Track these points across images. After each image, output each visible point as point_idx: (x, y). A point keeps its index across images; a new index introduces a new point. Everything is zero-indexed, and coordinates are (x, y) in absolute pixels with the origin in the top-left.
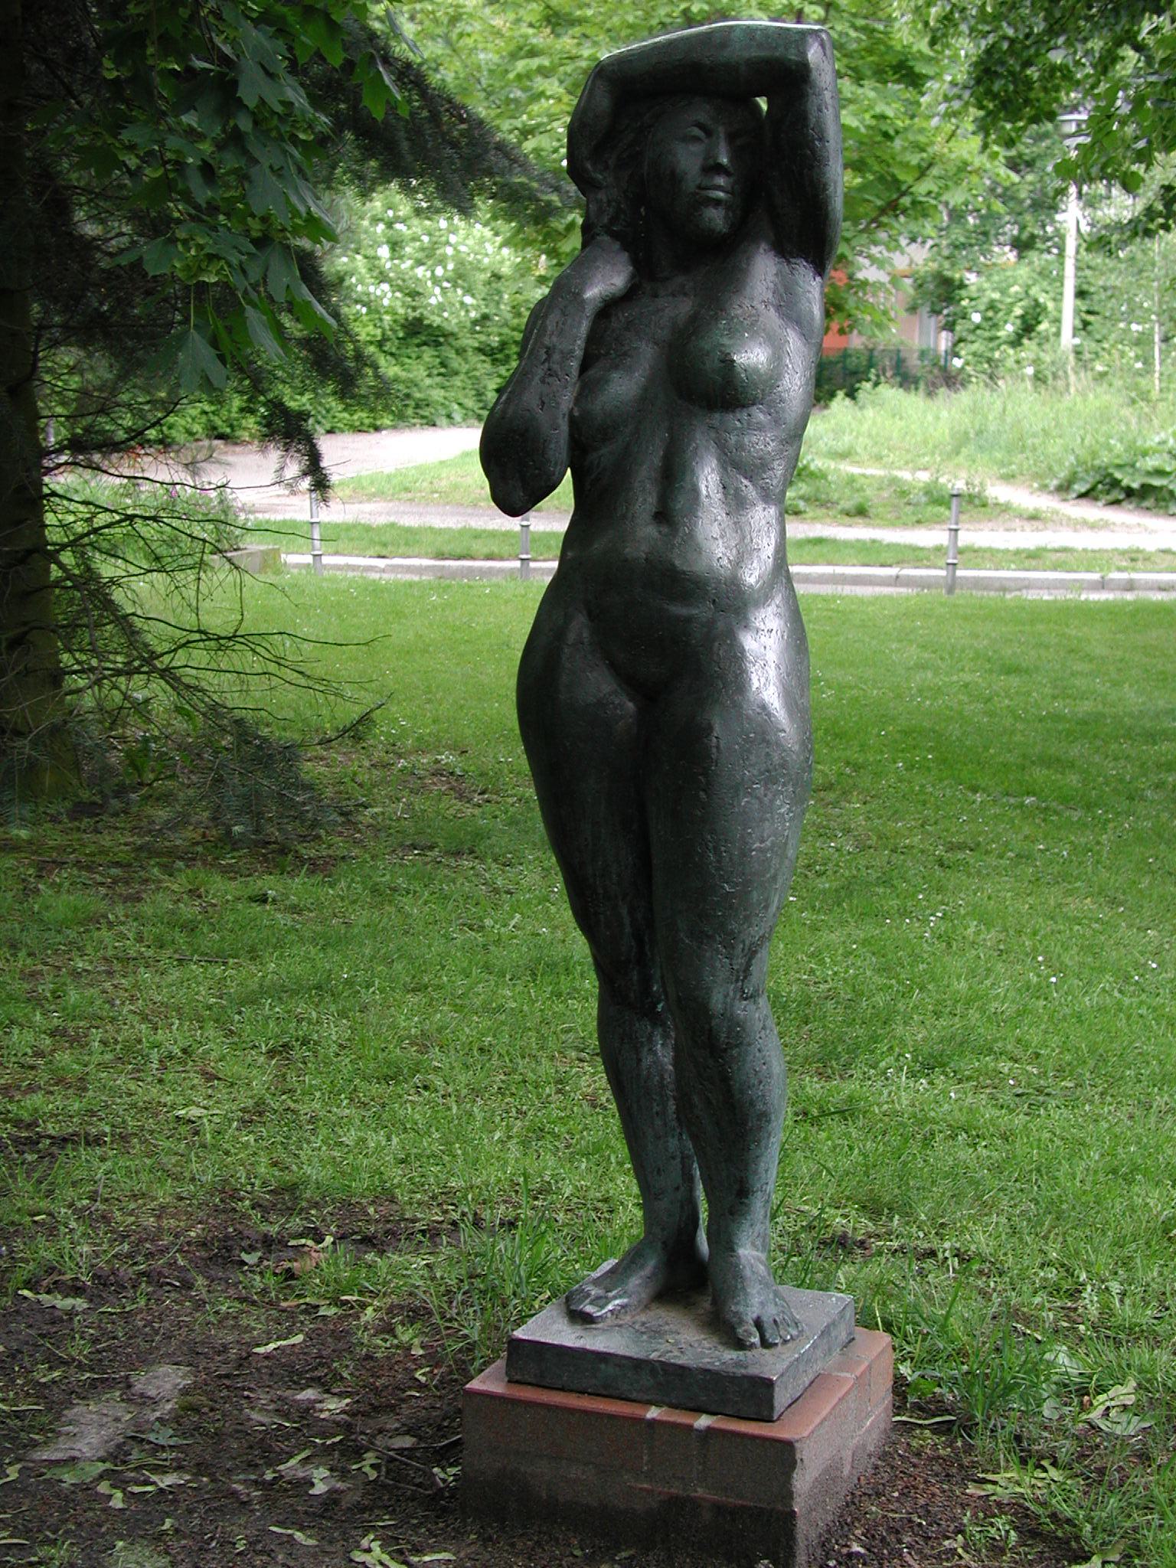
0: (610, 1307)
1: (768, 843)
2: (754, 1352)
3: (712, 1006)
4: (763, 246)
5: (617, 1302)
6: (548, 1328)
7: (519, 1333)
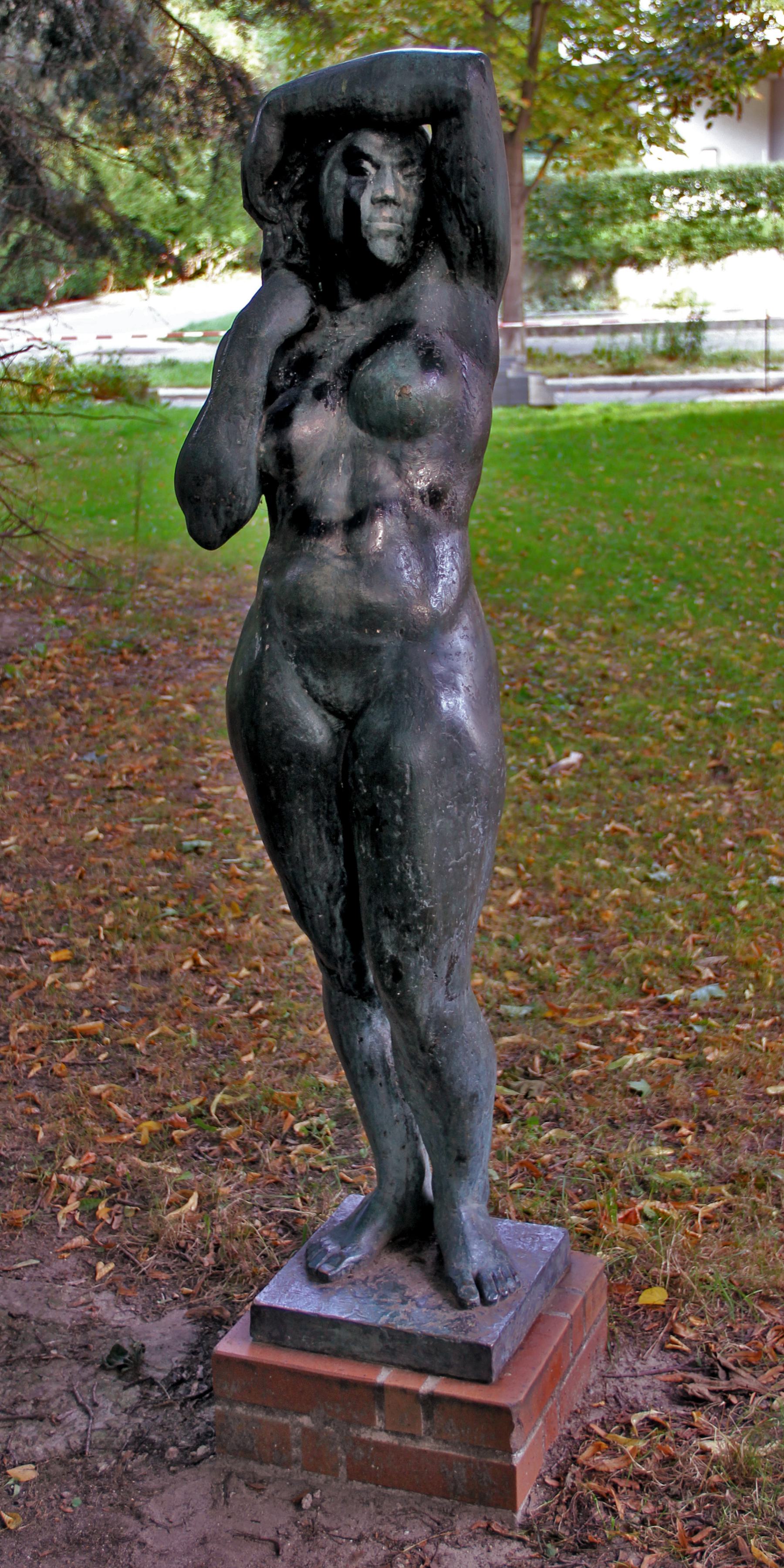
0: (343, 1265)
1: (464, 858)
2: (473, 1312)
3: (418, 1011)
4: (325, 752)
5: (352, 1258)
6: (290, 1293)
7: (262, 1299)
